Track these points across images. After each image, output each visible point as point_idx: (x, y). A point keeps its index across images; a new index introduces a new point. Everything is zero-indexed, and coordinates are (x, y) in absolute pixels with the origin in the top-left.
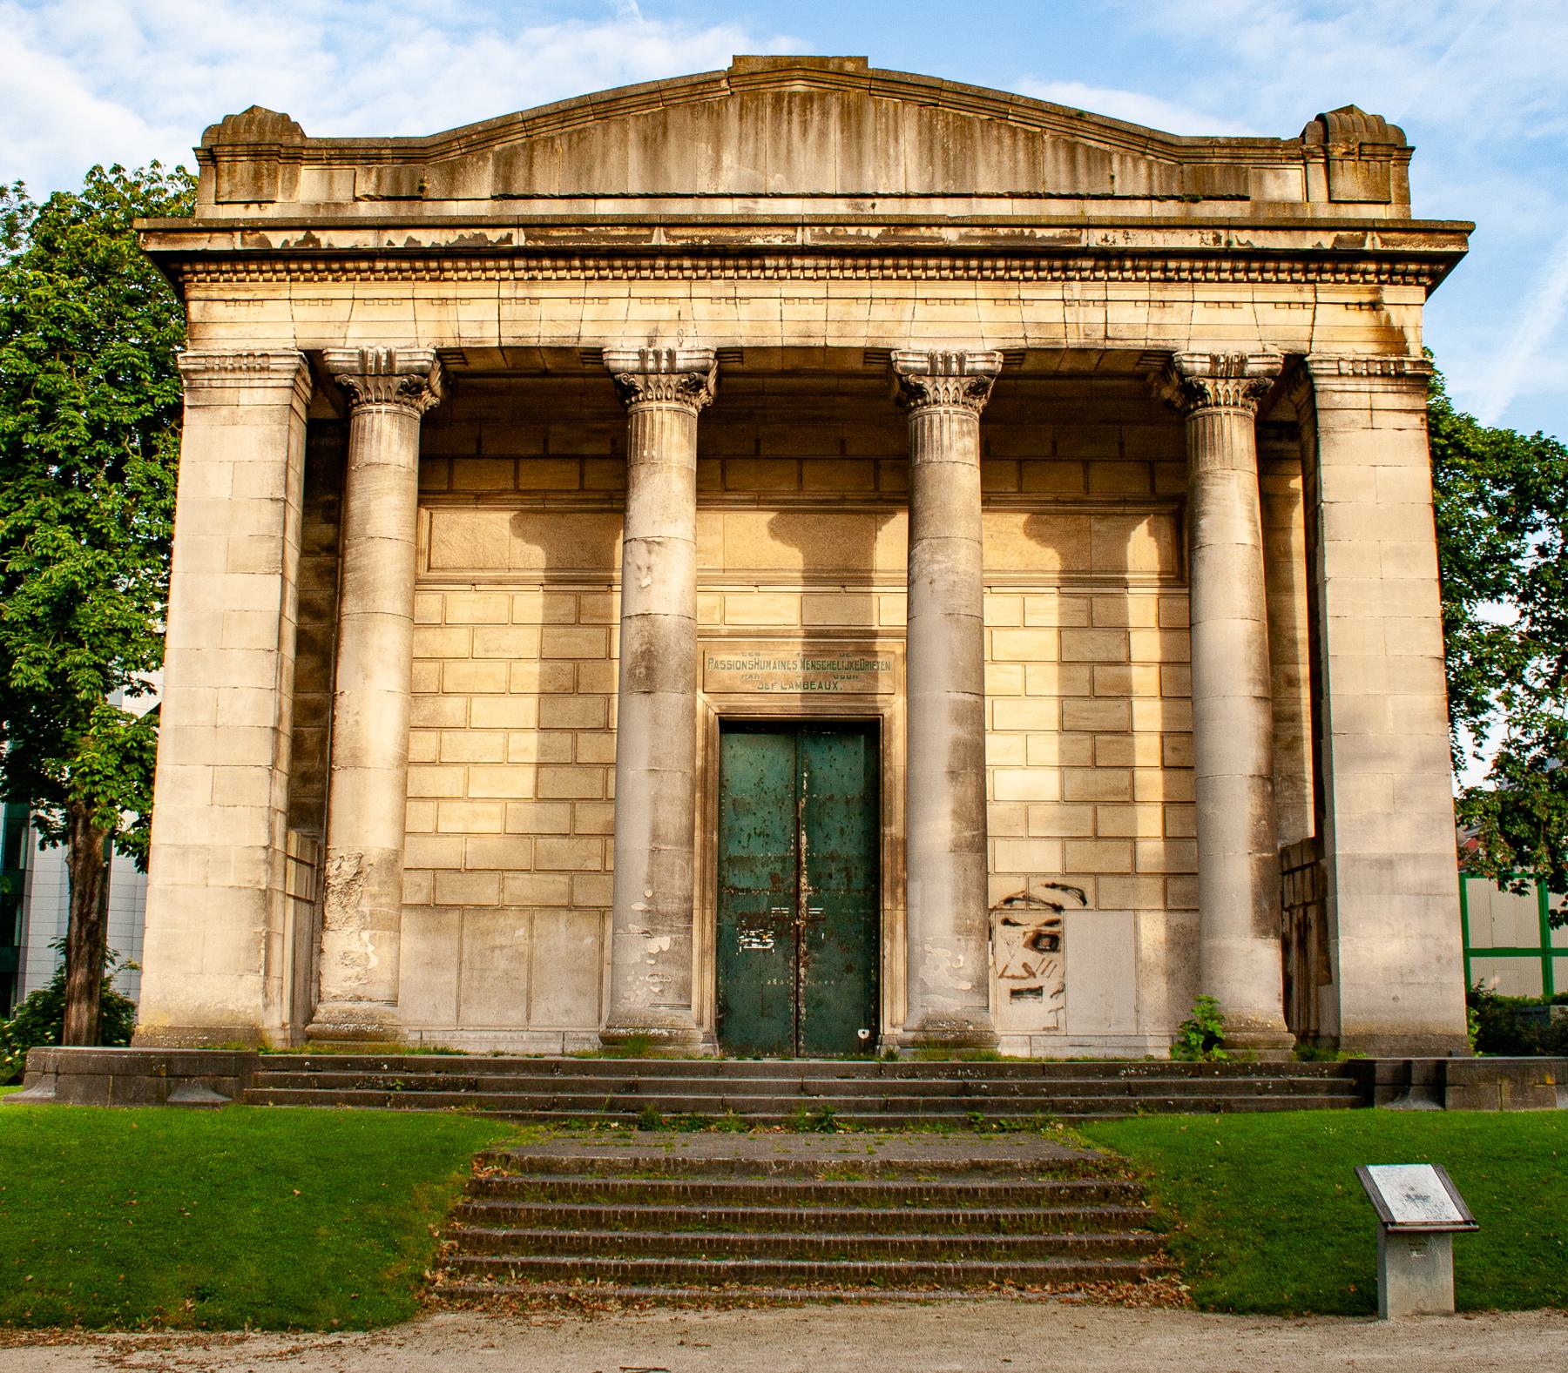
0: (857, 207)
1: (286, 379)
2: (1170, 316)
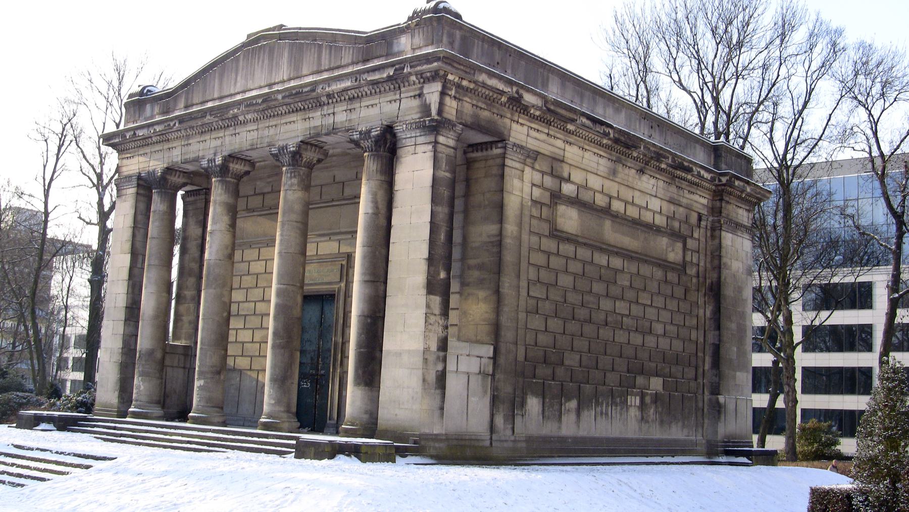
2: (354, 116)
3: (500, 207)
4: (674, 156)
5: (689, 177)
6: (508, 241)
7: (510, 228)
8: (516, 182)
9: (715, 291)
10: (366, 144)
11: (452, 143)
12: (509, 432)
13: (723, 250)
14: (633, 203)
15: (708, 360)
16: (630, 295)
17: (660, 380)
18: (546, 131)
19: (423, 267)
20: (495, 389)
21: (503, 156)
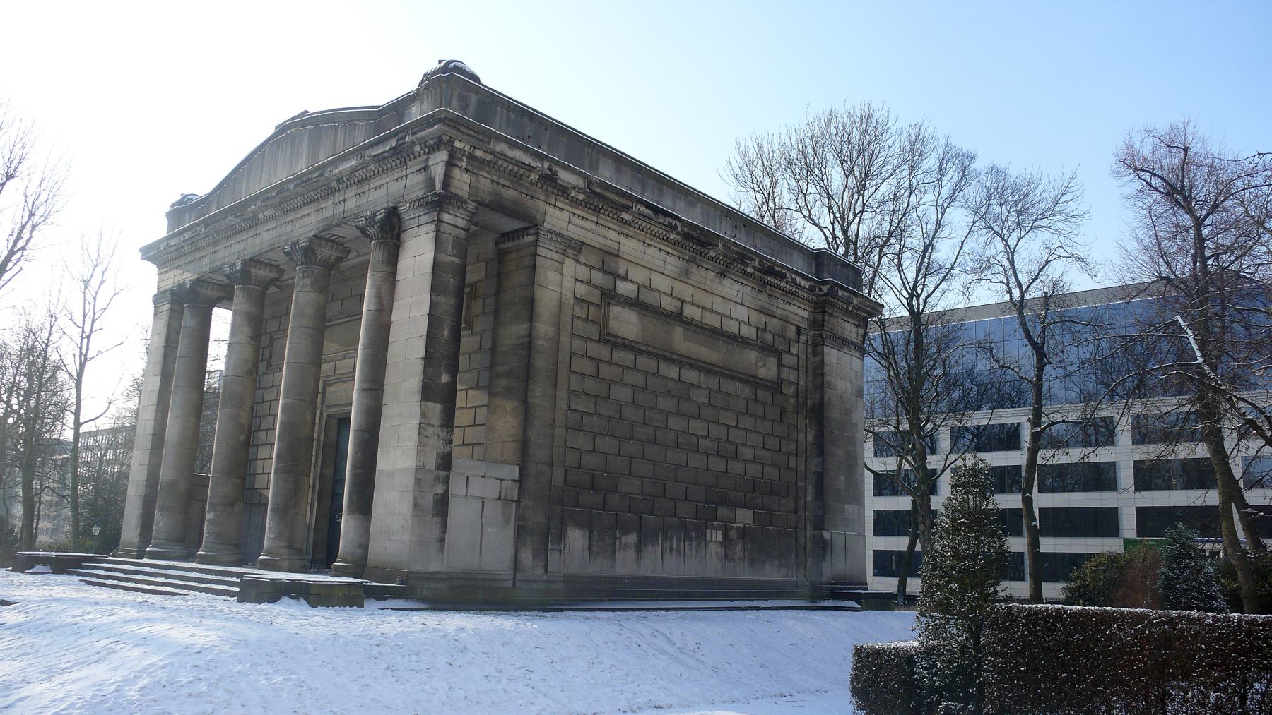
2: (363, 201)
3: (530, 306)
4: (762, 258)
5: (783, 284)
6: (540, 343)
7: (544, 328)
8: (553, 276)
9: (818, 413)
10: (372, 231)
11: (461, 223)
12: (540, 571)
13: (827, 368)
14: (712, 311)
15: (810, 490)
16: (708, 413)
17: (750, 513)
18: (595, 219)
19: (419, 368)
20: (520, 518)
21: (535, 244)
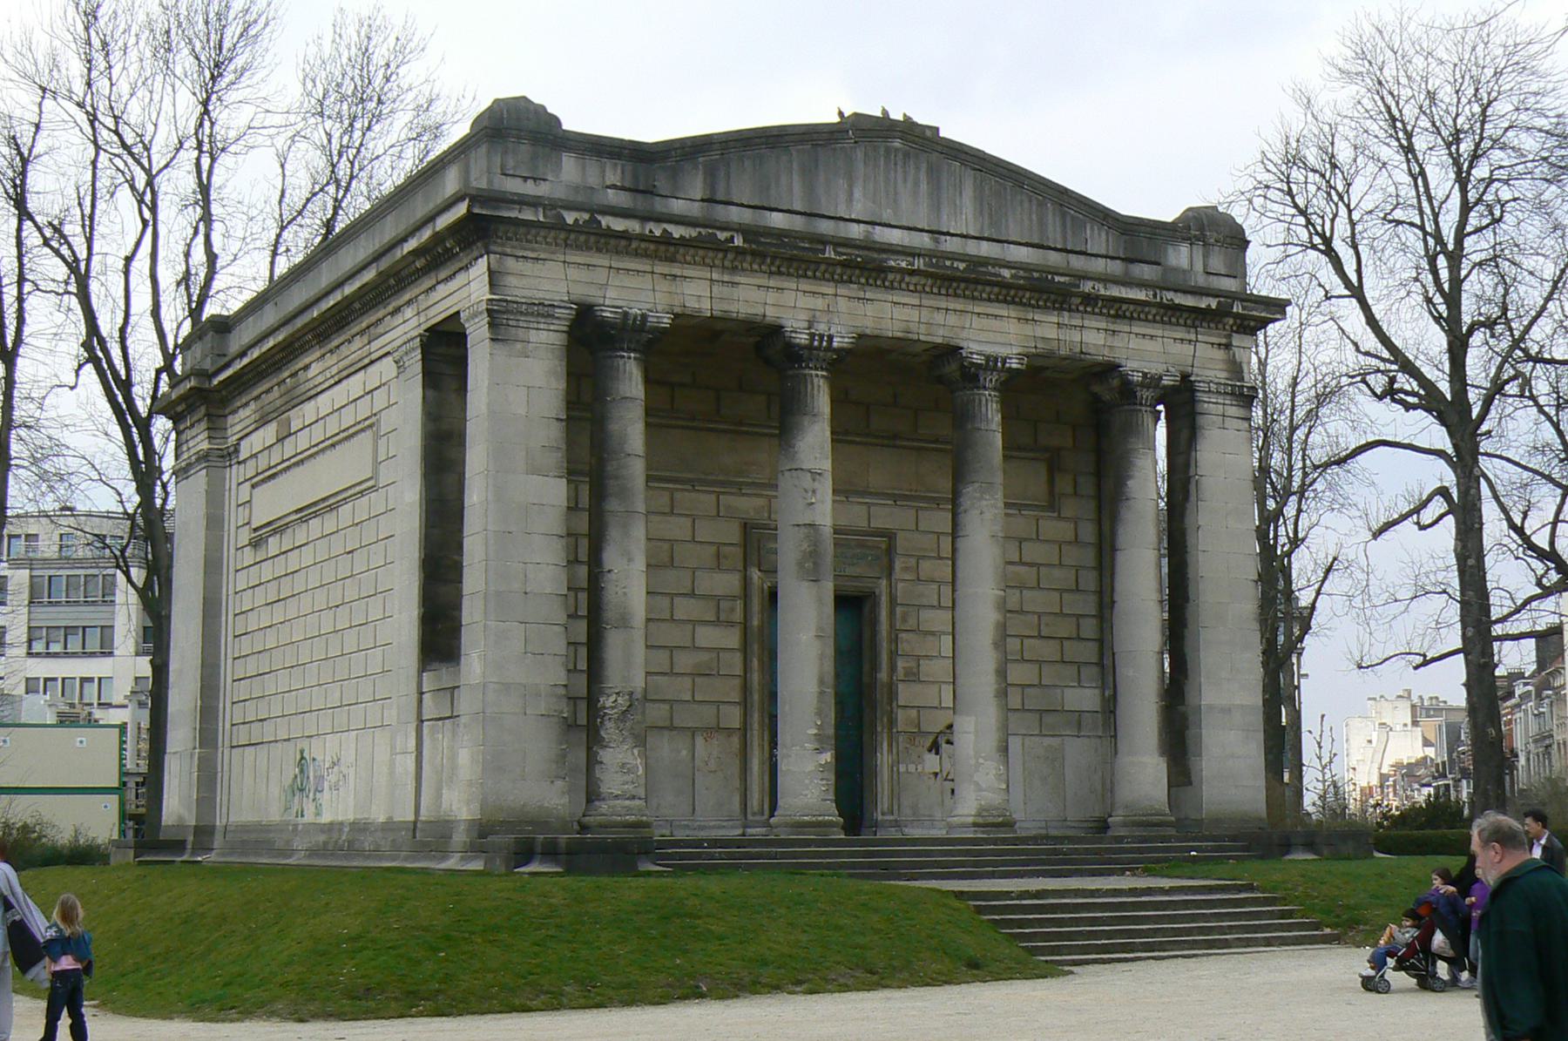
0: (937, 241)
1: (563, 326)
2: (1117, 342)
18: (562, 258)
